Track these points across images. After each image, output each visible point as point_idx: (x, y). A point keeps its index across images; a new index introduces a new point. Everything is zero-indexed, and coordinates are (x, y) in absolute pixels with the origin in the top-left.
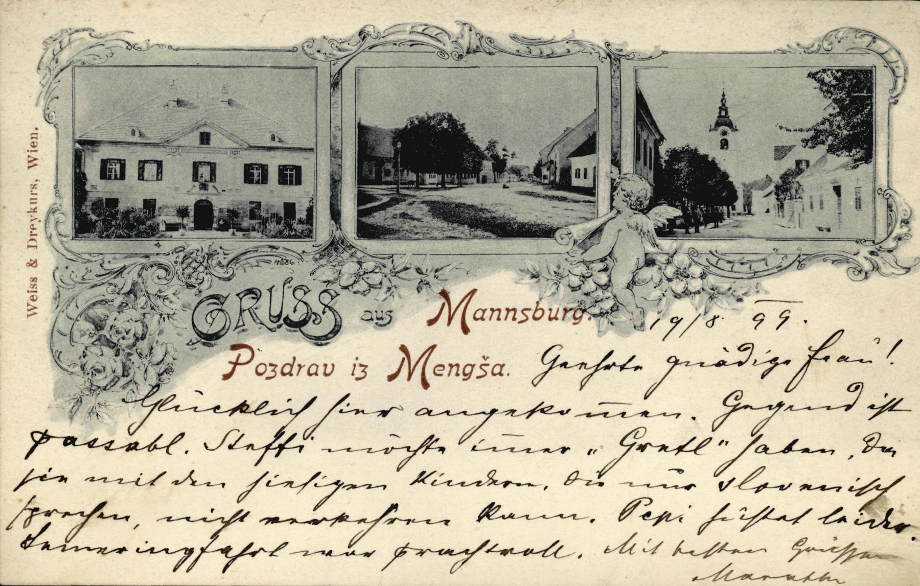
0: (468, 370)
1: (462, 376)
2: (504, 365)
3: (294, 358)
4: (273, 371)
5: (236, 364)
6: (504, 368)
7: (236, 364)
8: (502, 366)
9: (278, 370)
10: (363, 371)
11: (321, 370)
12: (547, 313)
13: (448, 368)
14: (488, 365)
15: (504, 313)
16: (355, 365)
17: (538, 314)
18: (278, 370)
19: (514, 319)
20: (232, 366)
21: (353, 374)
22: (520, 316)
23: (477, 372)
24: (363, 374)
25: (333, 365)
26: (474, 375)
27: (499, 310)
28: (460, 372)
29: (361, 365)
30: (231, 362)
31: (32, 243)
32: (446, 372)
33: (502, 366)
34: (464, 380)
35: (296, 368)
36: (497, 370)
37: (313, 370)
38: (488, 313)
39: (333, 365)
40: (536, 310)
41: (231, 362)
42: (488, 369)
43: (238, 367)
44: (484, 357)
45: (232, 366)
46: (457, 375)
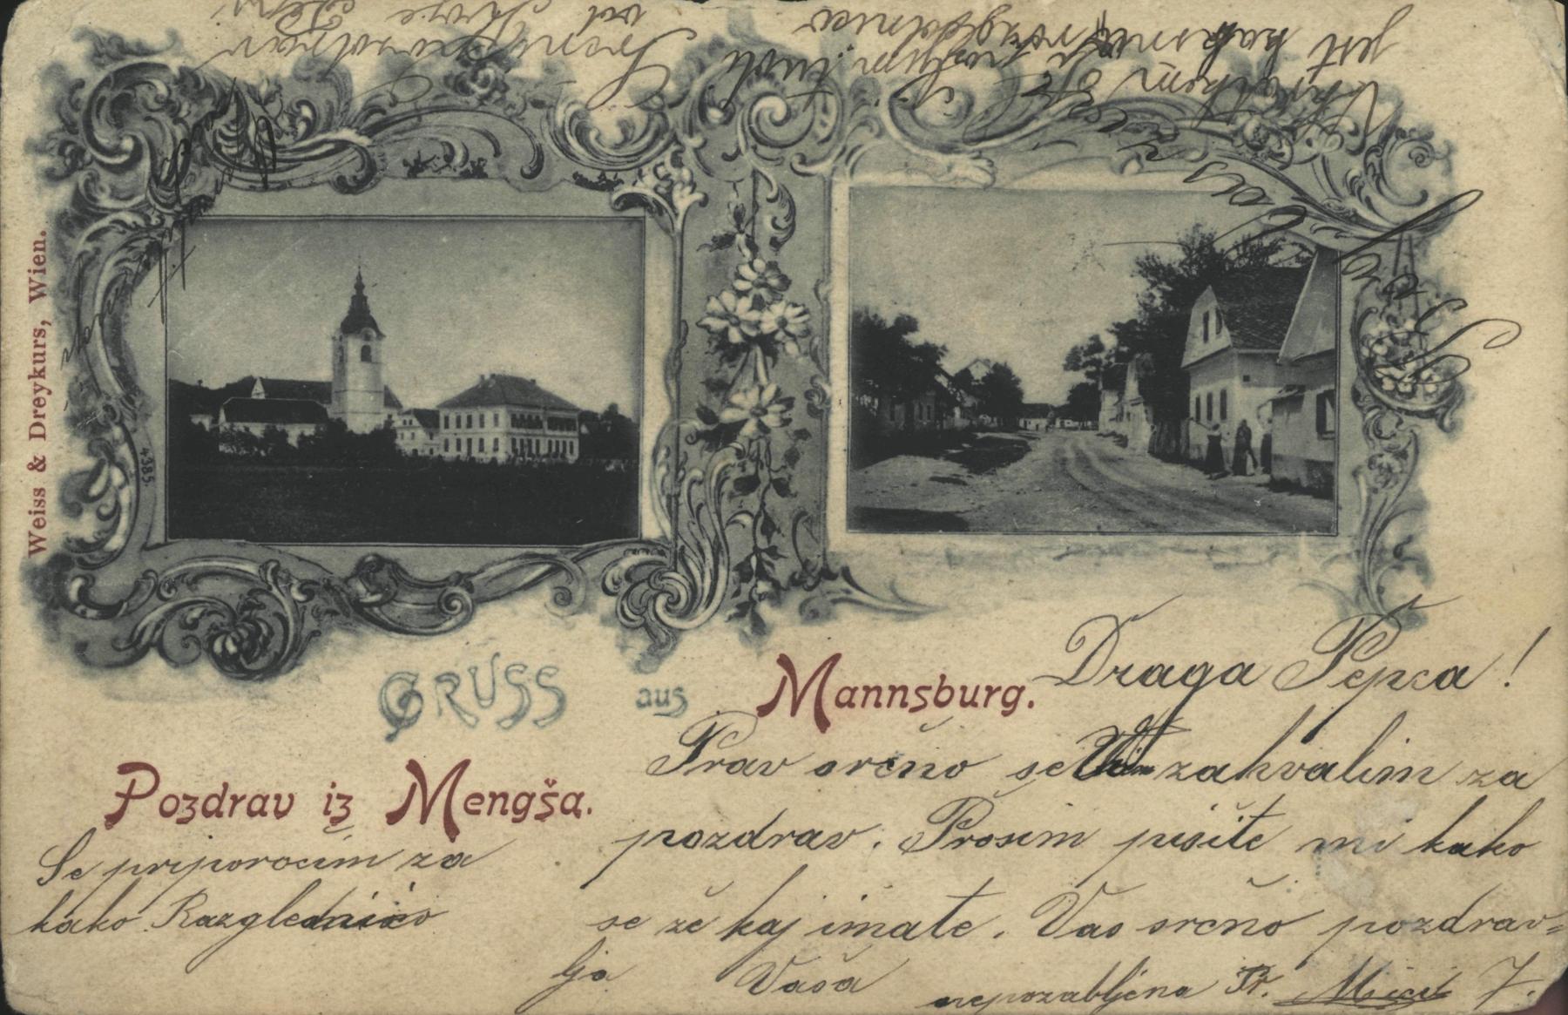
0: (523, 802)
1: (511, 815)
2: (582, 794)
3: (226, 786)
4: (190, 807)
5: (128, 797)
6: (583, 801)
7: (128, 797)
8: (579, 797)
9: (198, 807)
10: (344, 806)
11: (271, 805)
12: (958, 694)
13: (488, 801)
14: (555, 795)
15: (886, 694)
16: (330, 796)
17: (944, 696)
18: (198, 807)
19: (903, 704)
20: (120, 801)
21: (327, 812)
22: (913, 701)
23: (537, 807)
24: (343, 812)
25: (291, 797)
26: (533, 811)
27: (878, 689)
28: (509, 806)
29: (340, 797)
30: (118, 794)
31: (38, 430)
32: (484, 808)
33: (579, 797)
34: (515, 821)
35: (228, 803)
36: (570, 804)
37: (257, 805)
38: (860, 694)
39: (291, 797)
40: (941, 689)
41: (118, 794)
42: (555, 802)
43: (132, 804)
44: (547, 781)
45: (120, 801)
46: (504, 812)
